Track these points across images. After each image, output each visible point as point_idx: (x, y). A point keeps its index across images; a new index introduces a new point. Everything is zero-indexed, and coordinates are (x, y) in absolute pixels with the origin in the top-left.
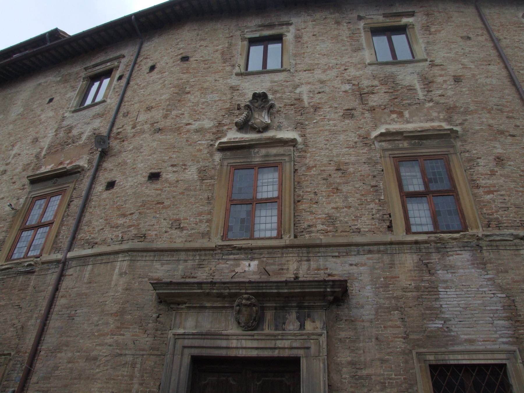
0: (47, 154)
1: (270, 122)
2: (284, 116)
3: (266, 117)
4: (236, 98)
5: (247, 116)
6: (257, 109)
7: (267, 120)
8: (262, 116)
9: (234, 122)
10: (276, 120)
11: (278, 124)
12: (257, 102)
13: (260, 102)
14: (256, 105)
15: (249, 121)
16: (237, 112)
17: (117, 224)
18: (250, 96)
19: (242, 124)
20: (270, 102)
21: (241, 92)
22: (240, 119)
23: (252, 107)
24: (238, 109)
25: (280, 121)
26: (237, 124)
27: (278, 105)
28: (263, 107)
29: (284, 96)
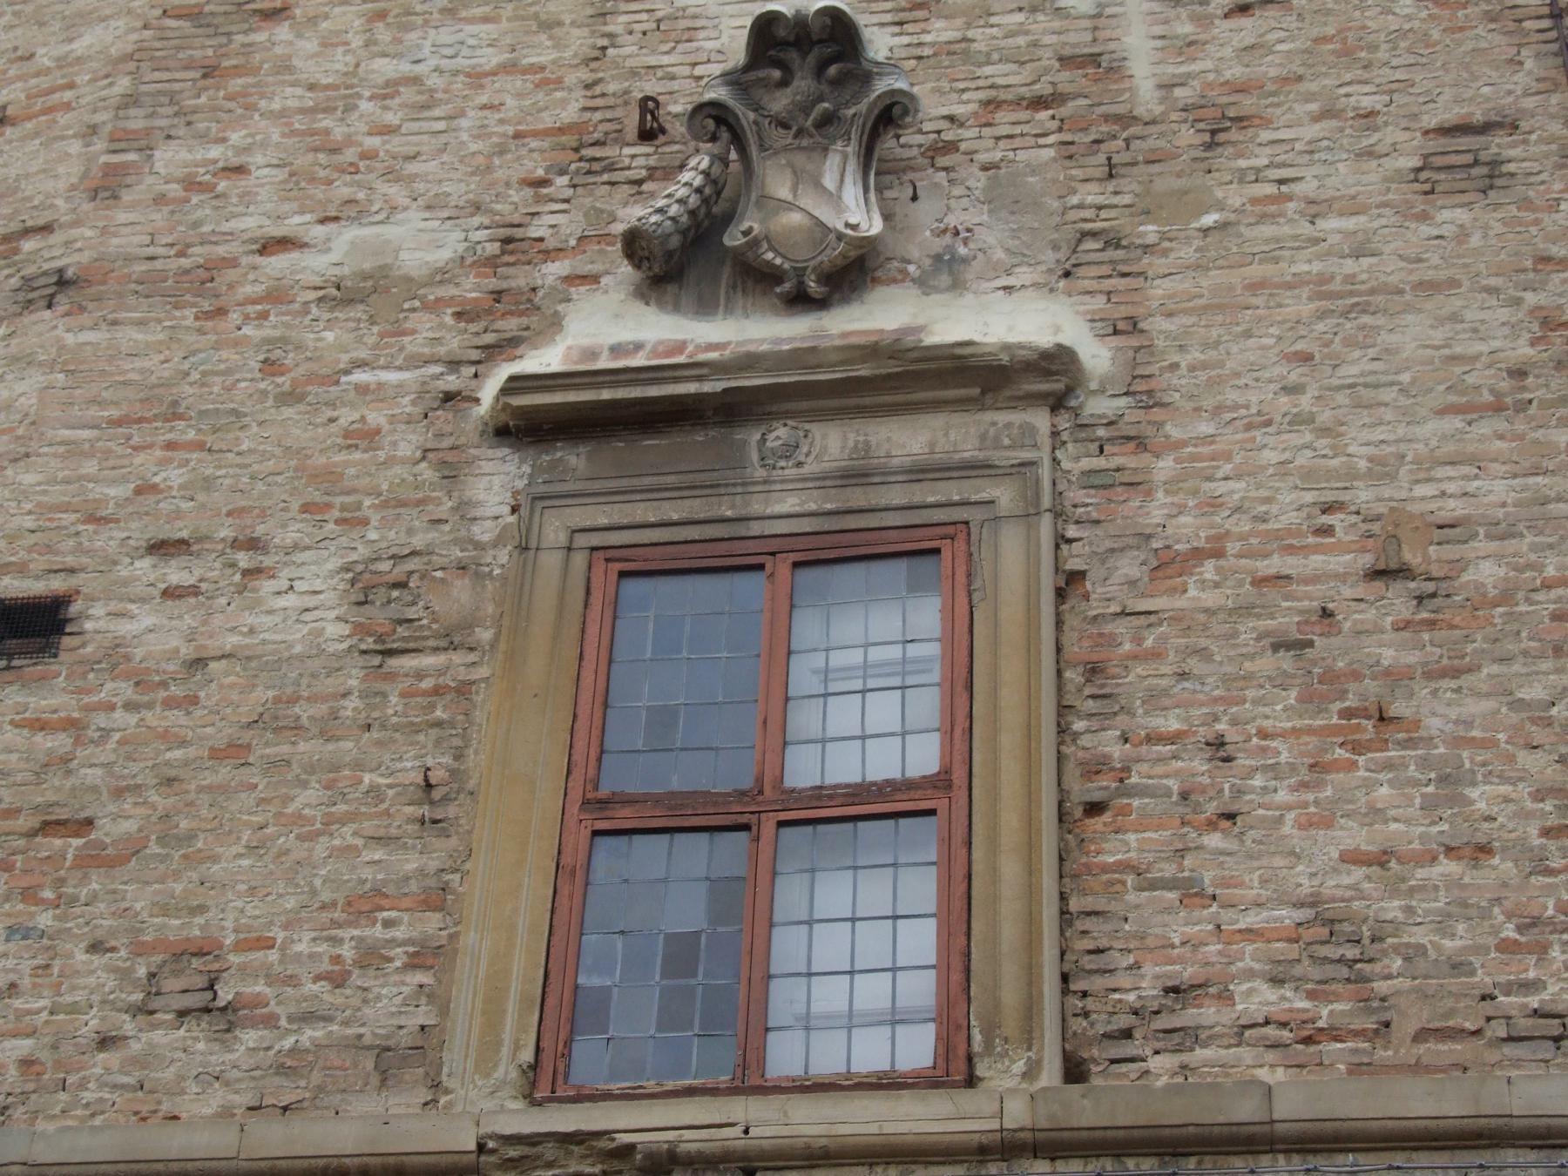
2: (978, 181)
3: (852, 193)
4: (628, 51)
7: (854, 211)
8: (818, 185)
9: (619, 228)
10: (926, 212)
11: (938, 244)
12: (784, 83)
13: (803, 84)
14: (779, 103)
15: (728, 218)
16: (637, 157)
18: (730, 41)
19: (675, 242)
20: (881, 86)
22: (664, 204)
23: (747, 117)
25: (952, 220)
26: (634, 244)
27: (935, 103)
28: (826, 121)
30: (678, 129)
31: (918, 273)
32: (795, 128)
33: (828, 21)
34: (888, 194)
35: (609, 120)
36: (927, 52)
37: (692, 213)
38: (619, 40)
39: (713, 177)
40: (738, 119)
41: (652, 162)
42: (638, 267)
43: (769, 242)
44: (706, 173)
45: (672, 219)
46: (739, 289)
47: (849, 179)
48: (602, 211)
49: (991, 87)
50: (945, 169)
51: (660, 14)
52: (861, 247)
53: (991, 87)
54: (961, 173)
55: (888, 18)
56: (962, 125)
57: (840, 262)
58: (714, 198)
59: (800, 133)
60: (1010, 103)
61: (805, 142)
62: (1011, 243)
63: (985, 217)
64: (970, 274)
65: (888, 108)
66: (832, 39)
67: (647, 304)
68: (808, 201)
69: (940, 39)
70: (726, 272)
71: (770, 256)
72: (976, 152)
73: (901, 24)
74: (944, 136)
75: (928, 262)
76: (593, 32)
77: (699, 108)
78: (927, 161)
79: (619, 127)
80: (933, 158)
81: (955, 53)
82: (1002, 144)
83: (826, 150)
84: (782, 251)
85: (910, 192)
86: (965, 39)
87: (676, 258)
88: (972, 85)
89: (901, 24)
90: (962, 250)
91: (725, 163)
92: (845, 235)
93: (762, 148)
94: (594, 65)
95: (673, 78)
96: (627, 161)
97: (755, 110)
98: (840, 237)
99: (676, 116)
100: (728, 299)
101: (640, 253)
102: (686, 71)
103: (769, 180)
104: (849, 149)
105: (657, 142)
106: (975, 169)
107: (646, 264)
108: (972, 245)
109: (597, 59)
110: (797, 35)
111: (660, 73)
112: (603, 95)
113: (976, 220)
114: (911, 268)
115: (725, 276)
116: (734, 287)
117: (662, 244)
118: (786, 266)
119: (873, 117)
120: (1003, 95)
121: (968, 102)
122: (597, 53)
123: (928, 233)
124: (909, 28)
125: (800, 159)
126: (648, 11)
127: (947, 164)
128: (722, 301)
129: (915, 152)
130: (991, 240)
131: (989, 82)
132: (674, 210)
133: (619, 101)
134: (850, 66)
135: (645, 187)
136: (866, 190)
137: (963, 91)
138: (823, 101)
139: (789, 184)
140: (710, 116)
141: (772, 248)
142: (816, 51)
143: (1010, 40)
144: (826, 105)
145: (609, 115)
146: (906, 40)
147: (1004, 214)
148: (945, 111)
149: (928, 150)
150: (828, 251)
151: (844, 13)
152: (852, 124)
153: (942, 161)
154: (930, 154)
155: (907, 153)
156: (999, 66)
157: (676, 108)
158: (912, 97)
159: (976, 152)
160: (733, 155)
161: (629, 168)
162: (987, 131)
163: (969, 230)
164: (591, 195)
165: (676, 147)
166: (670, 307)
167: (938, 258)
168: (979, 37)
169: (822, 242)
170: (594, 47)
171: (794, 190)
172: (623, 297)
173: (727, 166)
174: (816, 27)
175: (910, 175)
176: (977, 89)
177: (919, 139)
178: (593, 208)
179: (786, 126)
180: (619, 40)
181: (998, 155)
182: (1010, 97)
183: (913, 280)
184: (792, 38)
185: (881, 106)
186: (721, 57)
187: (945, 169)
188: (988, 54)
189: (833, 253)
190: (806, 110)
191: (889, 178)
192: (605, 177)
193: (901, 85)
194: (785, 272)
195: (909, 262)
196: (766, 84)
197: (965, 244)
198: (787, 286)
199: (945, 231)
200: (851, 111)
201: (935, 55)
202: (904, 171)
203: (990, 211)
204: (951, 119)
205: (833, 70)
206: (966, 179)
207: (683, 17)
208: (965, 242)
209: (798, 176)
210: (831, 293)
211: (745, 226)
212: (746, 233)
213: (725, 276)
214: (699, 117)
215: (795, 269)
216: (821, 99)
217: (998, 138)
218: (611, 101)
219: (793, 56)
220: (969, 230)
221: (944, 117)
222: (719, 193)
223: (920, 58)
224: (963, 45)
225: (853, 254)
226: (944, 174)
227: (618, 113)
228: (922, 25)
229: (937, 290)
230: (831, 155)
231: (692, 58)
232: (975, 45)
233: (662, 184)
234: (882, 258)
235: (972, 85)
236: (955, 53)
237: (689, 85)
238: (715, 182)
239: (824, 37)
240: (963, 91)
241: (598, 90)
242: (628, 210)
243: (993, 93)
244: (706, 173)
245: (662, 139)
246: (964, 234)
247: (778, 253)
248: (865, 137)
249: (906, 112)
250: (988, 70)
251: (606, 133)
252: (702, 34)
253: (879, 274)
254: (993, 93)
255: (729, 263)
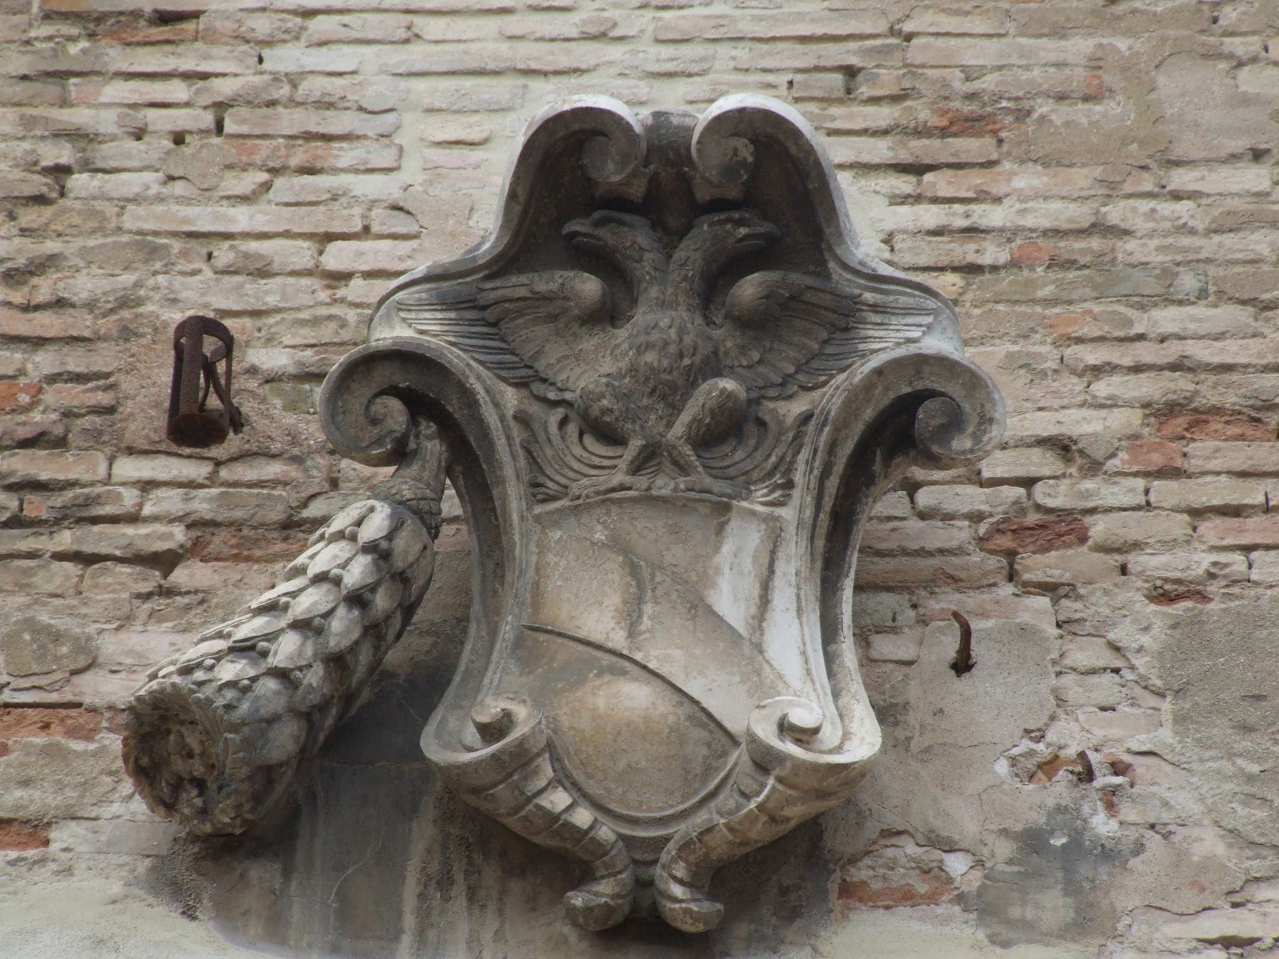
0: (633, 562)
1: (862, 740)
2: (1145, 630)
3: (790, 638)
4: (131, 182)
5: (397, 574)
6: (592, 467)
7: (796, 688)
8: (699, 609)
9: (115, 688)
10: (996, 707)
11: (1036, 802)
12: (607, 315)
13: (662, 321)
14: (594, 367)
15: (429, 685)
16: (160, 489)
17: (1230, 846)
18: (455, 185)
19: (284, 740)
20: (886, 343)
21: (233, 73)
22: (250, 631)
23: (497, 400)
24: (198, 422)
25: (1070, 736)
26: (161, 739)
27: (1041, 400)
28: (728, 428)
29: (1148, 227)
30: (270, 415)
31: (975, 880)
32: (636, 444)
33: (746, 152)
34: (885, 647)
35: (78, 378)
36: (992, 253)
37: (337, 662)
38: (106, 153)
39: (399, 564)
40: (471, 401)
41: (202, 504)
42: (166, 804)
43: (556, 760)
44: (379, 551)
45: (281, 674)
46: (459, 887)
47: (783, 597)
48: (57, 637)
49: (1175, 367)
50: (1048, 588)
51: (224, 88)
52: (822, 795)
53: (1175, 367)
54: (1096, 605)
55: (880, 150)
56: (1094, 467)
57: (760, 832)
58: (397, 622)
59: (648, 459)
60: (1234, 415)
61: (664, 485)
62: (1244, 815)
63: (1166, 735)
64: (1126, 893)
65: (907, 406)
66: (748, 202)
67: (189, 913)
68: (669, 651)
69: (1029, 221)
70: (422, 836)
71: (559, 800)
72: (1137, 546)
73: (917, 169)
74: (1041, 494)
75: (1004, 849)
76: (28, 123)
77: (367, 363)
78: (994, 562)
79: (104, 399)
80: (1011, 554)
81: (1070, 264)
82: (1211, 529)
83: (723, 509)
84: (592, 788)
85: (950, 646)
86: (1099, 228)
87: (280, 788)
88: (1125, 356)
89: (917, 169)
90: (1102, 825)
91: (431, 523)
92: (781, 758)
93: (537, 490)
94: (30, 217)
95: (264, 273)
96: (129, 498)
97: (521, 384)
98: (764, 761)
99: (272, 379)
100: (424, 915)
101: (178, 765)
102: (302, 254)
103: (553, 583)
104: (787, 513)
105: (216, 451)
106: (1133, 594)
107: (191, 796)
108: (1129, 812)
109: (40, 200)
110: (654, 180)
111: (224, 254)
112: (60, 304)
113: (1141, 741)
114: (957, 865)
115: (417, 850)
116: (445, 882)
117: (248, 744)
118: (606, 833)
119: (859, 428)
120: (1210, 393)
121: (1111, 404)
122: (38, 183)
123: (1002, 767)
124: (938, 182)
125: (646, 531)
126: (188, 76)
127: (1056, 575)
128: (409, 920)
129: (961, 533)
130: (1185, 802)
131: (1172, 351)
132: (287, 649)
133: (107, 325)
134: (798, 279)
135: (180, 576)
136: (830, 633)
137: (1097, 371)
138: (719, 374)
139: (614, 600)
140: (393, 391)
141: (563, 779)
142: (704, 228)
143: (1229, 240)
144: (728, 384)
145: (75, 361)
146: (931, 216)
147: (1220, 729)
148: (1044, 425)
149: (998, 530)
150: (727, 799)
151: (795, 132)
152: (797, 444)
153: (1041, 565)
154: (1005, 542)
155: (937, 536)
156: (1198, 310)
157: (275, 359)
158: (973, 380)
159: (1137, 546)
160: (451, 504)
161: (133, 518)
162: (1164, 491)
163: (1118, 768)
164: (22, 587)
165: (273, 469)
166: (255, 928)
167: (1032, 842)
168: (1142, 225)
169: (708, 771)
170: (31, 165)
171: (631, 617)
172: (116, 888)
173: (434, 532)
174: (708, 167)
175: (948, 600)
176: (1137, 369)
177: (970, 497)
178: (29, 624)
179: (611, 436)
180: (106, 153)
181: (1202, 561)
182: (1231, 399)
183: (961, 899)
184: (637, 190)
185: (883, 398)
186: (401, 224)
187: (1048, 588)
188: (1168, 274)
189: (737, 809)
190: (671, 393)
191: (888, 601)
192: (65, 539)
193: (937, 343)
194: (601, 850)
195: (951, 847)
196: (552, 310)
197: (1110, 807)
198: (604, 891)
199: (1049, 766)
200: (797, 407)
201: (1014, 264)
202: (932, 583)
203: (1180, 719)
204: (1062, 447)
205: (749, 288)
206: (1107, 623)
207: (292, 103)
208: (1110, 800)
209: (641, 581)
210: (725, 922)
211: (491, 708)
212: (492, 732)
213: (417, 850)
214: (361, 392)
215: (628, 841)
216: (713, 366)
217: (1197, 513)
218: (82, 324)
219: (636, 239)
220: (1118, 768)
221: (1043, 442)
222: (408, 610)
223: (972, 270)
224: (1095, 243)
225: (797, 812)
226: (1044, 602)
227: (104, 359)
228: (977, 178)
229: (1030, 931)
230: (734, 524)
231: (318, 220)
232: (1131, 245)
233: (234, 572)
234: (872, 829)
235: (1125, 356)
236: (1070, 264)
237: (310, 293)
238: (402, 578)
239: (734, 193)
240: (1097, 371)
241: (44, 288)
242: (133, 639)
243: (1182, 384)
244: (379, 551)
245: (234, 443)
246: (1104, 779)
247: (582, 795)
248: (833, 483)
249: (954, 422)
250: (1167, 319)
251: (68, 414)
252: (346, 155)
253: (861, 873)
254: (1182, 384)
255: (429, 810)
